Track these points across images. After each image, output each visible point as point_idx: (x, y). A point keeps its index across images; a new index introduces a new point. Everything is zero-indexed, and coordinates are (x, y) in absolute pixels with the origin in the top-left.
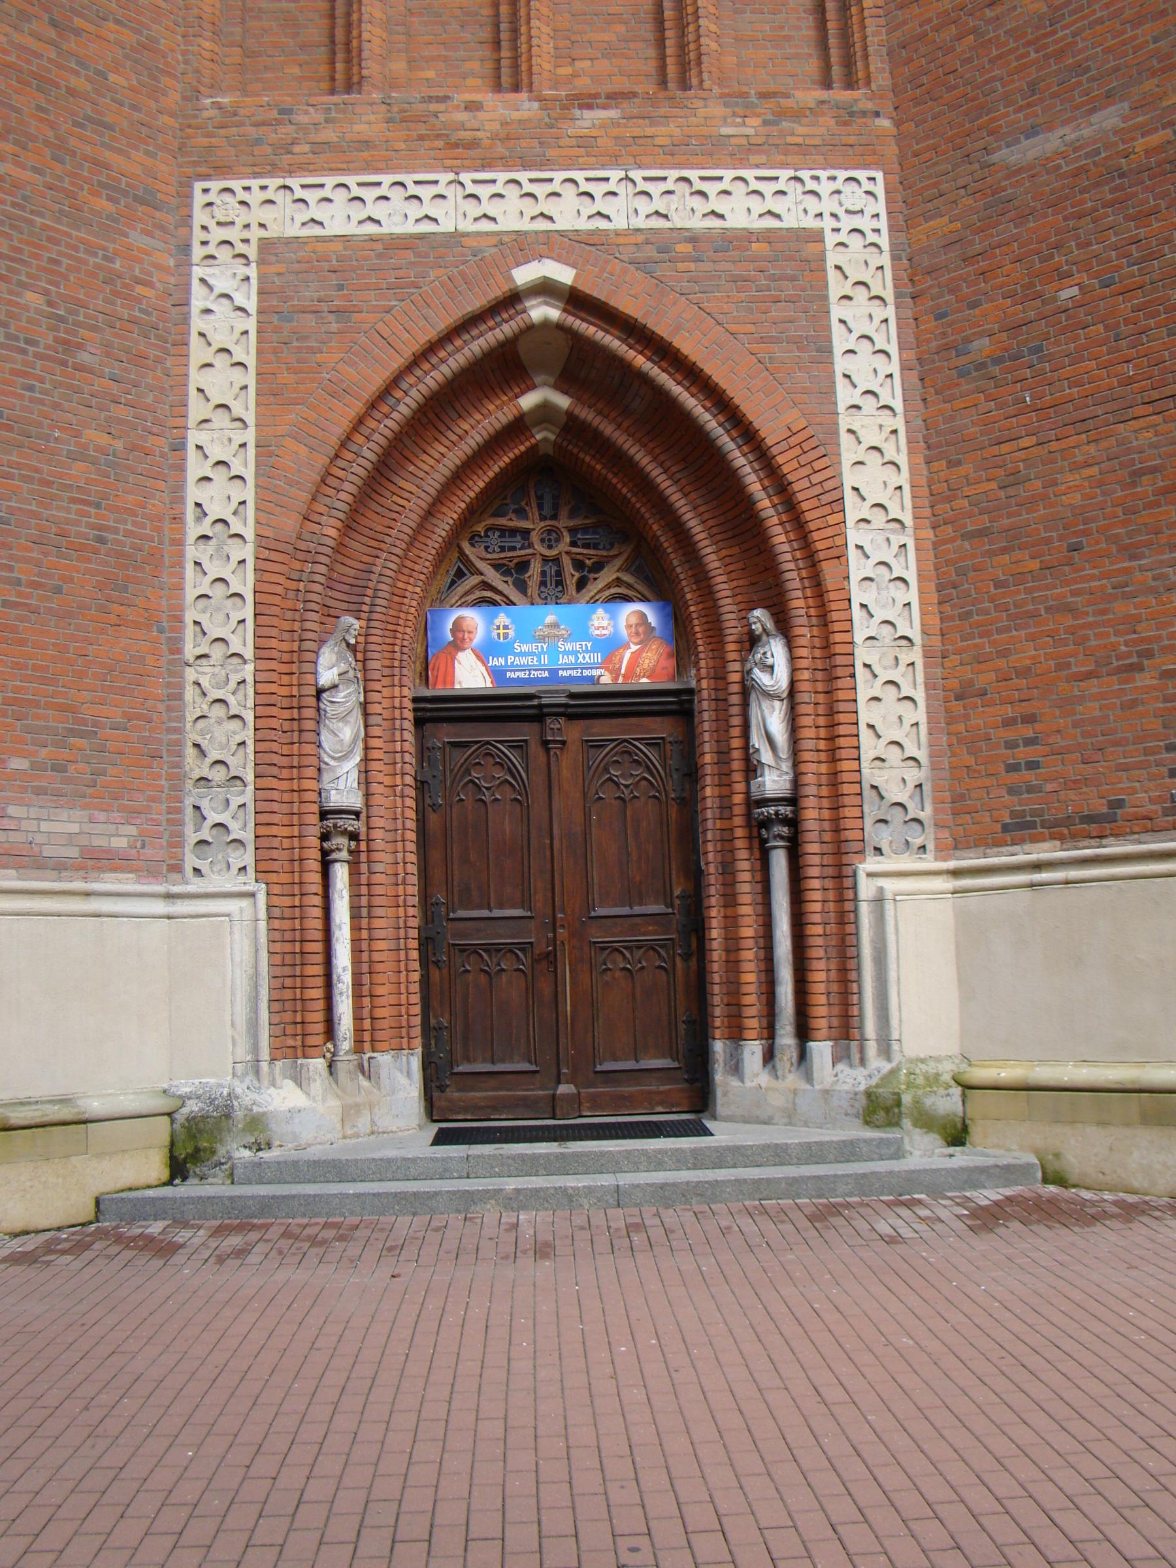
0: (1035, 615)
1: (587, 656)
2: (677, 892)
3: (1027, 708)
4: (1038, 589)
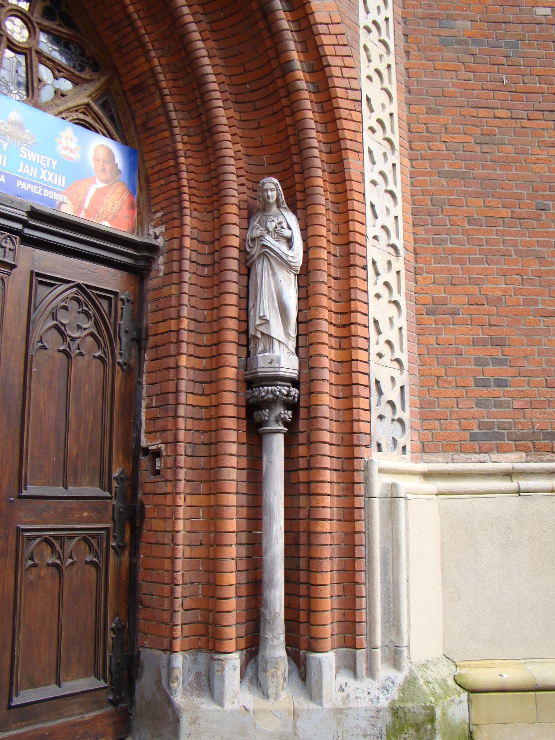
0: (506, 254)
1: (51, 175)
2: (116, 474)
3: (496, 332)
4: (509, 234)
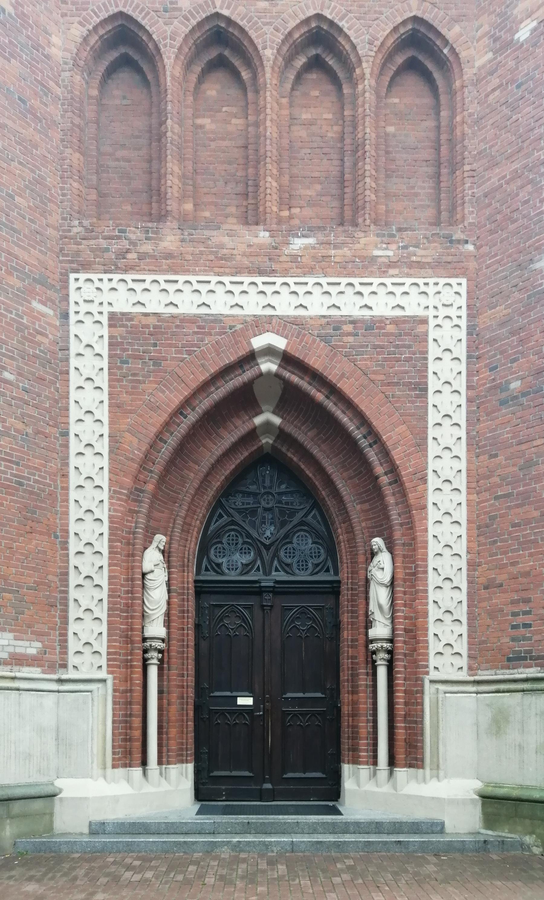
0: (535, 542)
3: (525, 595)
